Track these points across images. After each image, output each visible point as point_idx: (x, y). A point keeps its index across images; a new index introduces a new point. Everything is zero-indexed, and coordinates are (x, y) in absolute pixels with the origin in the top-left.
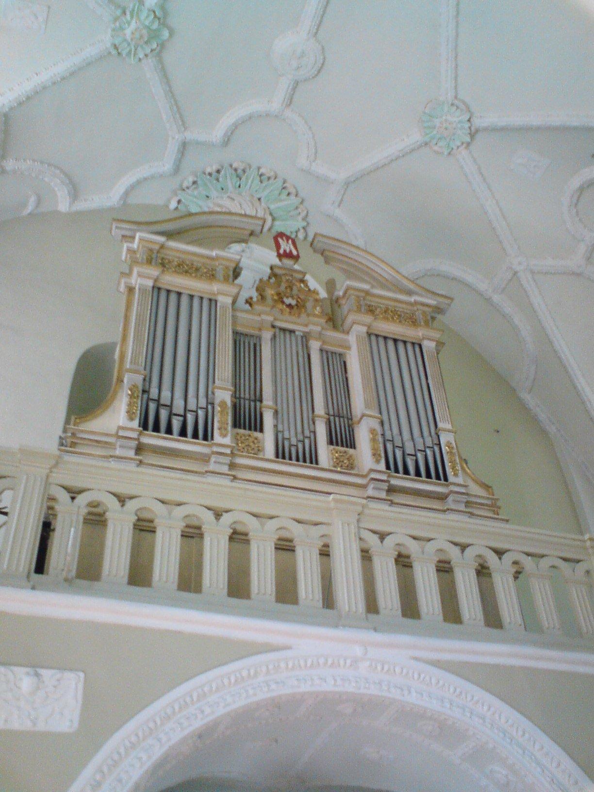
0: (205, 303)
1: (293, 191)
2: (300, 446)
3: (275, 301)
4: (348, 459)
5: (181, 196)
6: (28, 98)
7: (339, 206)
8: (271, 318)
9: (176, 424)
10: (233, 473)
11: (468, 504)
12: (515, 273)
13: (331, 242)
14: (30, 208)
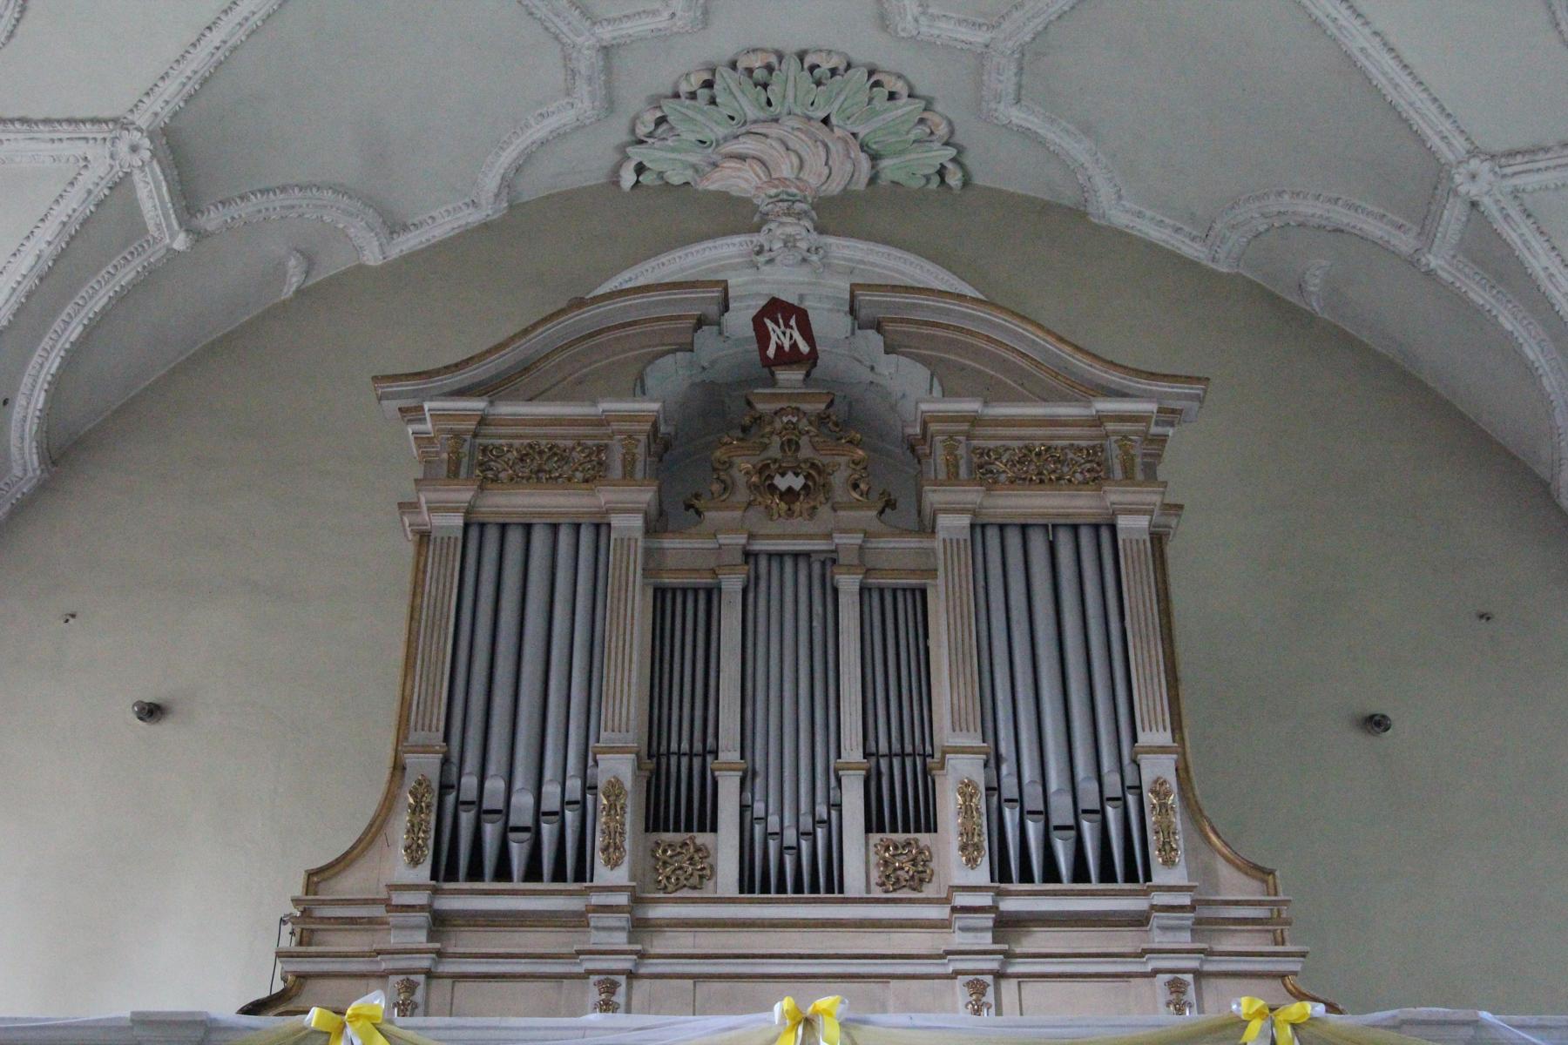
0: (586, 537)
1: (899, 87)
2: (805, 846)
3: (753, 488)
4: (914, 861)
5: (637, 154)
6: (205, 82)
7: (1018, 101)
8: (742, 540)
9: (518, 854)
10: (638, 947)
11: (1201, 926)
12: (1474, 204)
13: (898, 299)
14: (294, 281)
